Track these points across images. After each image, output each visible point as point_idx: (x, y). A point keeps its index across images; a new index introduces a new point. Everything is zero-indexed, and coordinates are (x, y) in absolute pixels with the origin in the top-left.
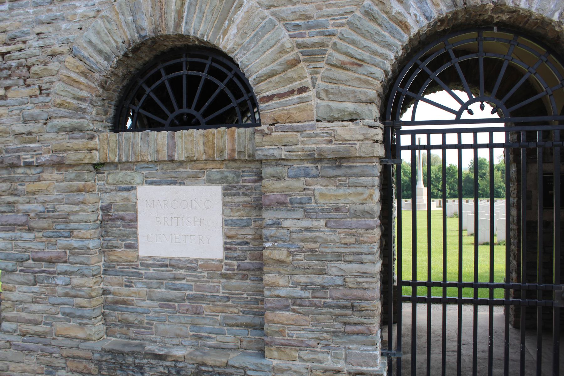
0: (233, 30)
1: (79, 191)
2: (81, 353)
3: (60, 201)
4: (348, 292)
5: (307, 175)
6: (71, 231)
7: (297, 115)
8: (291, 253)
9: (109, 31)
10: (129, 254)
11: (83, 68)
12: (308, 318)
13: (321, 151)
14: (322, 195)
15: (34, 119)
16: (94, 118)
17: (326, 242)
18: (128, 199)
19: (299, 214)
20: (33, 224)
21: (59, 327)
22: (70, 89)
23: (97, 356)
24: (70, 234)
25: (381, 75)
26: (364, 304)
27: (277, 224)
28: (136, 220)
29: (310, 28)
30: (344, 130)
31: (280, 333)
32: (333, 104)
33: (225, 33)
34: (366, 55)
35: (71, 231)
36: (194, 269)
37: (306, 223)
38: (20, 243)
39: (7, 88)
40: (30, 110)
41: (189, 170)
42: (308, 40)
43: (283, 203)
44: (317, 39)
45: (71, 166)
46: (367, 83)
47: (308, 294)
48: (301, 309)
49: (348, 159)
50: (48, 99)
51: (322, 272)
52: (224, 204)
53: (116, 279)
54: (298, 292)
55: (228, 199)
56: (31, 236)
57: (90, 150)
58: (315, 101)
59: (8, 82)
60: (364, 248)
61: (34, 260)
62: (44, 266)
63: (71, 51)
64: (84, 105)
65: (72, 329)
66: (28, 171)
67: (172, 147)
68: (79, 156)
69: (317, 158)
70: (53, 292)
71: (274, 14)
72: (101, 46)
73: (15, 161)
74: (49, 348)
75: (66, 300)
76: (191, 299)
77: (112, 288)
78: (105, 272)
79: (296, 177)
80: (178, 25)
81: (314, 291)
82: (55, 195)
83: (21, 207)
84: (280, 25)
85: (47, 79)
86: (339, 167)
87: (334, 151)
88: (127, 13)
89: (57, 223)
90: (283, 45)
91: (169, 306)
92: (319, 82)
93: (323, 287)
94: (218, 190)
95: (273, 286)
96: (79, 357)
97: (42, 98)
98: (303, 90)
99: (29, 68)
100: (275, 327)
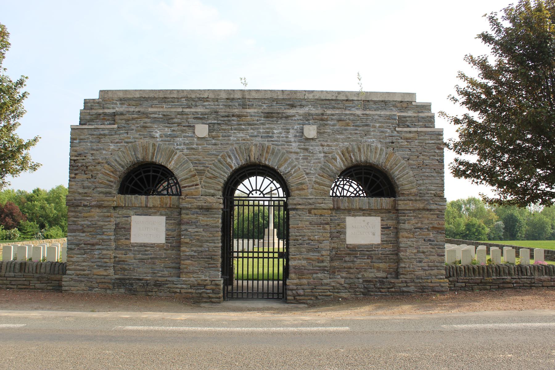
0: (173, 162)
1: (108, 217)
2: (106, 281)
3: (99, 221)
4: (210, 253)
5: (197, 214)
6: (103, 232)
7: (194, 193)
8: (191, 240)
9: (124, 157)
10: (127, 242)
11: (112, 170)
12: (196, 263)
13: (202, 205)
14: (202, 220)
15: (89, 188)
16: (114, 190)
17: (203, 236)
18: (127, 221)
19: (194, 227)
20: (85, 230)
21: (95, 271)
22: (106, 177)
23: (113, 281)
24: (103, 233)
25: (222, 181)
26: (215, 257)
27: (186, 230)
28: (130, 229)
29: (200, 164)
30: (210, 199)
31: (186, 268)
32: (206, 190)
33: (170, 163)
34: (218, 175)
35: (103, 232)
36: (153, 247)
37: (196, 230)
38: (78, 237)
39: (76, 174)
40: (86, 184)
41: (153, 210)
42: (199, 168)
43: (188, 223)
44: (202, 168)
45: (105, 207)
46: (218, 184)
47: (196, 254)
48: (194, 260)
49: (211, 209)
50: (95, 180)
51: (201, 246)
52: (166, 223)
53: (120, 252)
54: (193, 253)
55: (168, 221)
56: (84, 234)
57: (114, 201)
58: (201, 189)
59: (77, 172)
60: (216, 238)
61: (85, 244)
62: (89, 247)
63: (107, 162)
64: (112, 184)
65: (102, 272)
66: (85, 208)
67: (147, 201)
68: (110, 203)
69: (201, 208)
70: (93, 257)
71: (188, 158)
72: (121, 162)
73: (79, 204)
74: (91, 280)
75: (99, 260)
76: (151, 258)
77: (118, 256)
78: (115, 249)
79: (193, 214)
80: (152, 158)
81: (198, 253)
82: (97, 218)
83: (80, 223)
84: (190, 162)
85: (95, 172)
86: (208, 211)
87: (207, 206)
88: (132, 151)
89: (97, 229)
90: (190, 169)
91: (142, 262)
92: (202, 183)
93: (202, 252)
94: (164, 218)
95: (184, 251)
96: (105, 282)
97: (92, 180)
98: (197, 185)
99: (87, 167)
100: (184, 266)
